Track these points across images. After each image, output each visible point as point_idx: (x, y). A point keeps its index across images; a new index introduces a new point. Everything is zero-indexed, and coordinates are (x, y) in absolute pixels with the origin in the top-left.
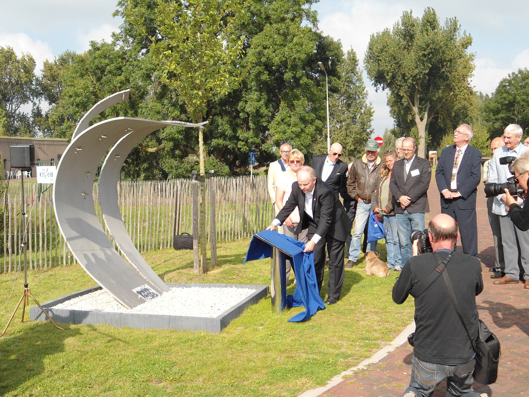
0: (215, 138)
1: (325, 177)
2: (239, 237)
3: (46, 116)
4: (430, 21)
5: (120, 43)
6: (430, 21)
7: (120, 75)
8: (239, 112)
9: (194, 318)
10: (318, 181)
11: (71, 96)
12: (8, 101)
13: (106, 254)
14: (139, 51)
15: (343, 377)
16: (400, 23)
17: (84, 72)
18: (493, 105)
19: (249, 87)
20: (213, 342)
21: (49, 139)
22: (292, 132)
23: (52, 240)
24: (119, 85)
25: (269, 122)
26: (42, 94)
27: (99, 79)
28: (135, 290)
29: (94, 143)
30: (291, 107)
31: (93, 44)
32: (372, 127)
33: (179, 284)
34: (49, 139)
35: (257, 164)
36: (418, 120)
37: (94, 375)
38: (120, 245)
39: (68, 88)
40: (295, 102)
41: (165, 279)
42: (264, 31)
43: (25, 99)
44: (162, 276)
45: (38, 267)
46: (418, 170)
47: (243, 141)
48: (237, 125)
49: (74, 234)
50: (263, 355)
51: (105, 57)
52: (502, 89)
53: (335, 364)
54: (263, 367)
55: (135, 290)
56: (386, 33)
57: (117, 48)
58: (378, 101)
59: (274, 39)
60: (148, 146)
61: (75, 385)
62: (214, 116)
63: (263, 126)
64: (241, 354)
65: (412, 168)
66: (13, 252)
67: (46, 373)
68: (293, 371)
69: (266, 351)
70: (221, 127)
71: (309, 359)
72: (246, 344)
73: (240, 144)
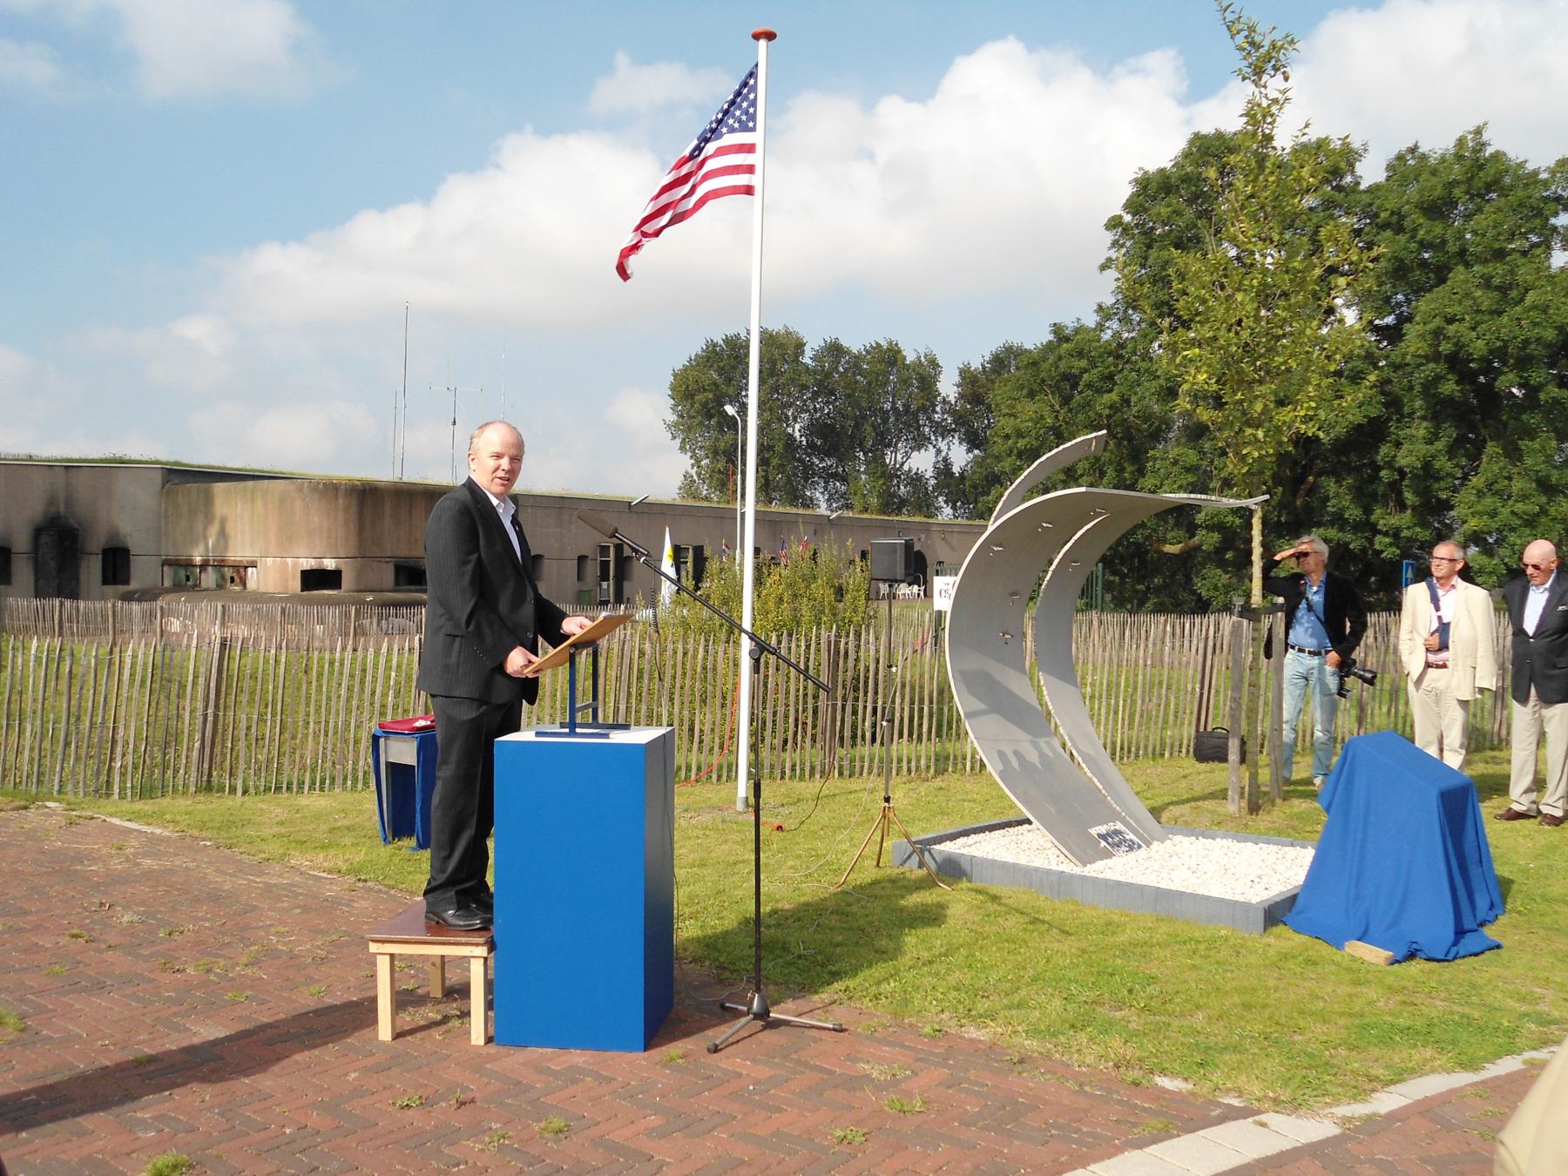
1: (1530, 625)
3: (961, 474)
5: (1114, 325)
7: (1111, 391)
8: (1380, 468)
9: (1209, 898)
10: (1519, 632)
11: (1007, 437)
12: (889, 446)
13: (1042, 755)
15: (1525, 1062)
17: (1035, 387)
19: (1406, 410)
20: (1243, 951)
21: (965, 522)
22: (1513, 513)
23: (946, 725)
24: (1107, 411)
25: (1455, 490)
26: (954, 430)
27: (1066, 401)
28: (1094, 831)
29: (1030, 538)
30: (1513, 453)
31: (1057, 329)
33: (1191, 830)
34: (965, 522)
37: (994, 977)
38: (1071, 739)
39: (1003, 421)
40: (1524, 444)
41: (1164, 819)
42: (1449, 283)
43: (920, 443)
44: (1156, 812)
45: (914, 771)
47: (1386, 534)
48: (1374, 497)
49: (980, 706)
50: (1349, 989)
51: (1081, 354)
53: (1513, 1033)
54: (1342, 1014)
55: (1094, 831)
57: (1107, 336)
59: (1474, 299)
60: (1165, 541)
61: (957, 989)
62: (1319, 475)
63: (1438, 499)
64: (1300, 982)
66: (874, 740)
67: (906, 960)
69: (1357, 983)
70: (1334, 501)
71: (1452, 1013)
72: (1315, 963)
73: (1380, 542)
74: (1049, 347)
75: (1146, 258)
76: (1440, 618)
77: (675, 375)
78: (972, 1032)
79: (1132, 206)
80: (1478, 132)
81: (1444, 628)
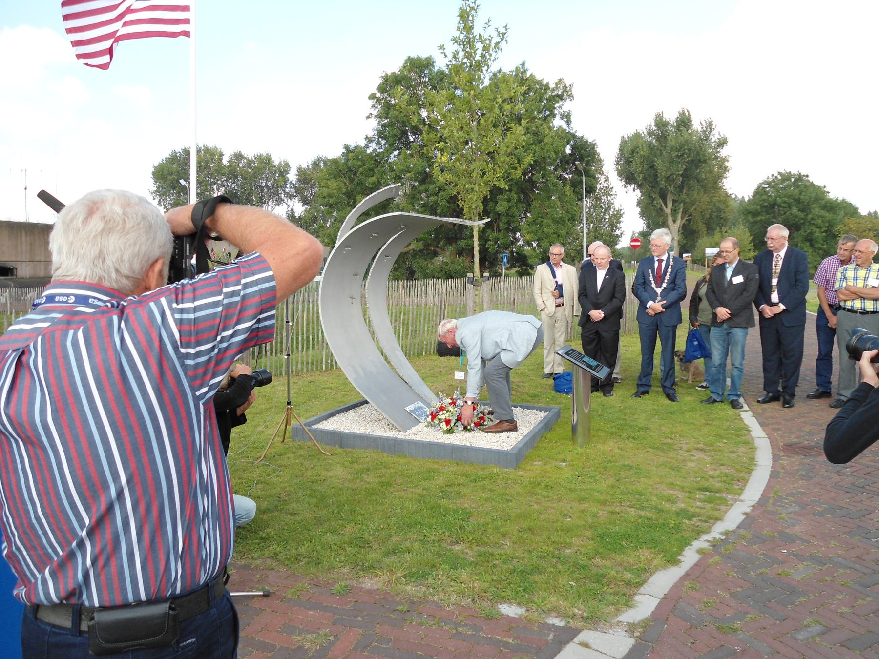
0: (465, 239)
4: (684, 121)
5: (373, 145)
6: (684, 121)
14: (392, 153)
16: (653, 124)
18: (752, 208)
27: (352, 180)
31: (346, 147)
35: (508, 265)
36: (670, 219)
43: (279, 202)
51: (358, 159)
52: (760, 192)
53: (678, 528)
56: (637, 135)
57: (369, 151)
58: (626, 200)
61: (350, 543)
68: (627, 536)
69: (581, 500)
71: (640, 517)
74: (343, 154)
75: (387, 114)
78: (368, 583)
79: (382, 89)
80: (523, 64)
81: (559, 287)
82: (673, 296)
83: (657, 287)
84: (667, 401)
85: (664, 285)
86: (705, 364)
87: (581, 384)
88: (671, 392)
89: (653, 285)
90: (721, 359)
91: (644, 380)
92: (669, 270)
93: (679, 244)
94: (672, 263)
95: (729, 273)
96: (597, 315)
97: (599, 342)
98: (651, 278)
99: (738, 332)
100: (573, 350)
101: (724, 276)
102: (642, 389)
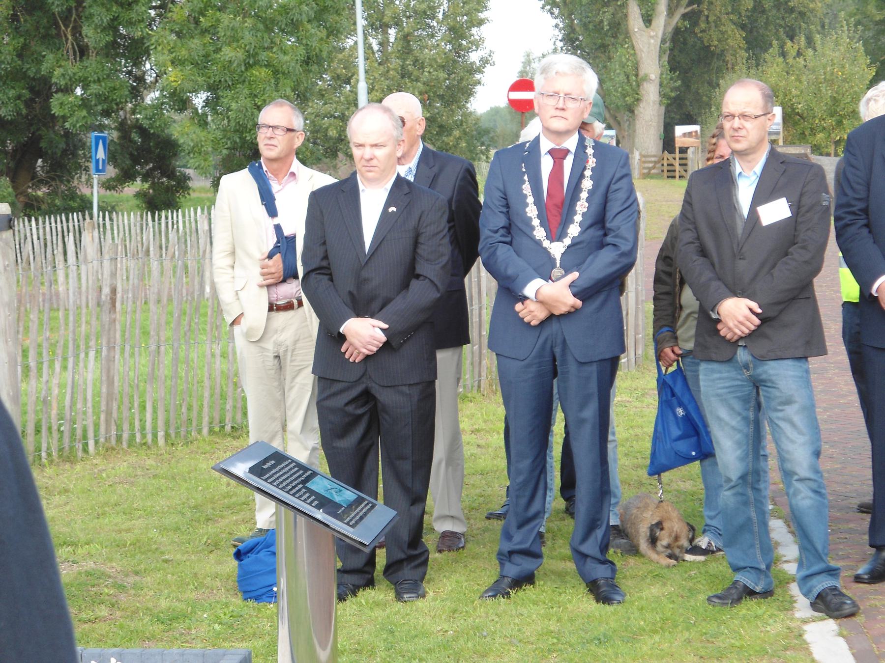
2: (91, 443)
32: (489, 45)
36: (635, 21)
46: (784, 200)
65: (762, 196)
76: (278, 228)
77: (777, 544)
82: (602, 263)
83: (551, 238)
84: (588, 605)
85: (574, 230)
86: (705, 475)
87: (300, 569)
88: (600, 572)
89: (540, 233)
90: (742, 459)
91: (518, 537)
92: (587, 184)
93: (663, 95)
94: (592, 162)
95: (745, 192)
96: (365, 333)
97: (376, 425)
98: (532, 211)
99: (783, 374)
100: (279, 457)
101: (732, 206)
102: (513, 570)
